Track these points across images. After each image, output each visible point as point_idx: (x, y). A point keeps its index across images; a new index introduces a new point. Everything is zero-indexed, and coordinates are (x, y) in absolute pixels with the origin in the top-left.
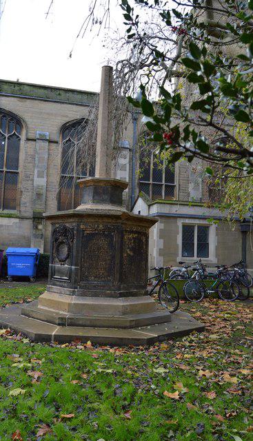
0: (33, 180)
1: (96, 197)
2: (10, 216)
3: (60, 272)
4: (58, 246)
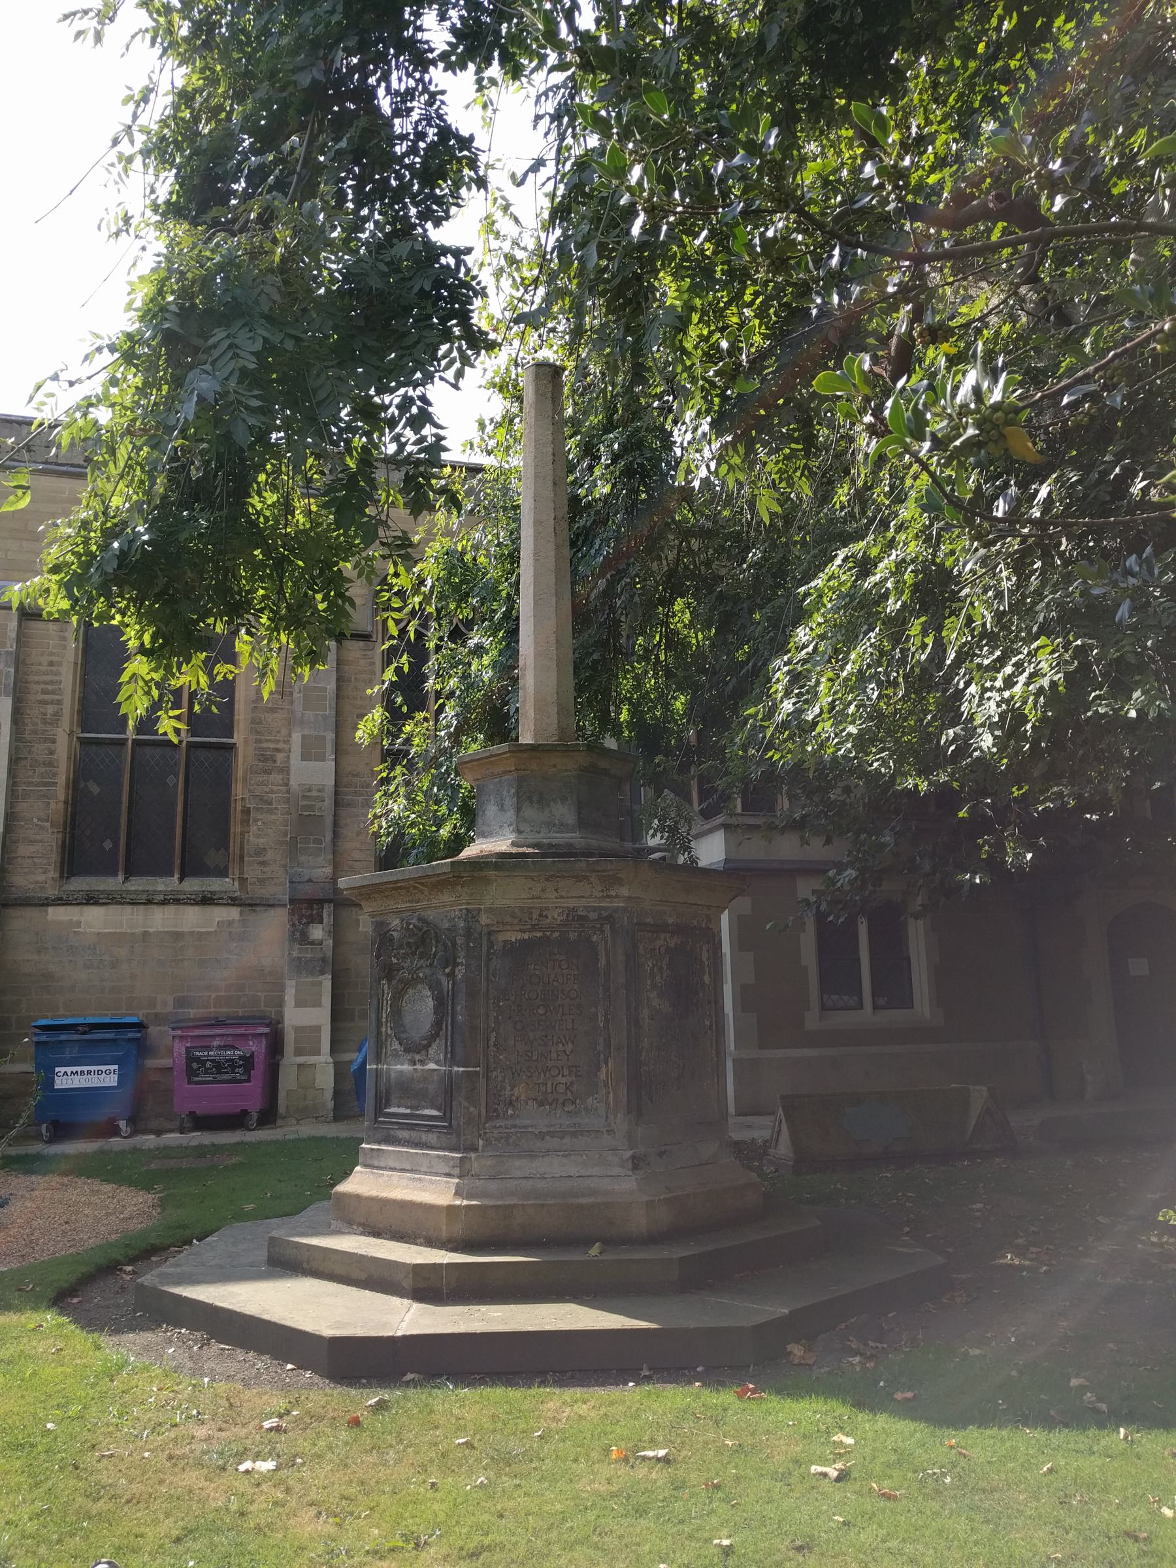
0: (285, 770)
1: (529, 812)
2: (207, 900)
3: (409, 1090)
4: (398, 995)
